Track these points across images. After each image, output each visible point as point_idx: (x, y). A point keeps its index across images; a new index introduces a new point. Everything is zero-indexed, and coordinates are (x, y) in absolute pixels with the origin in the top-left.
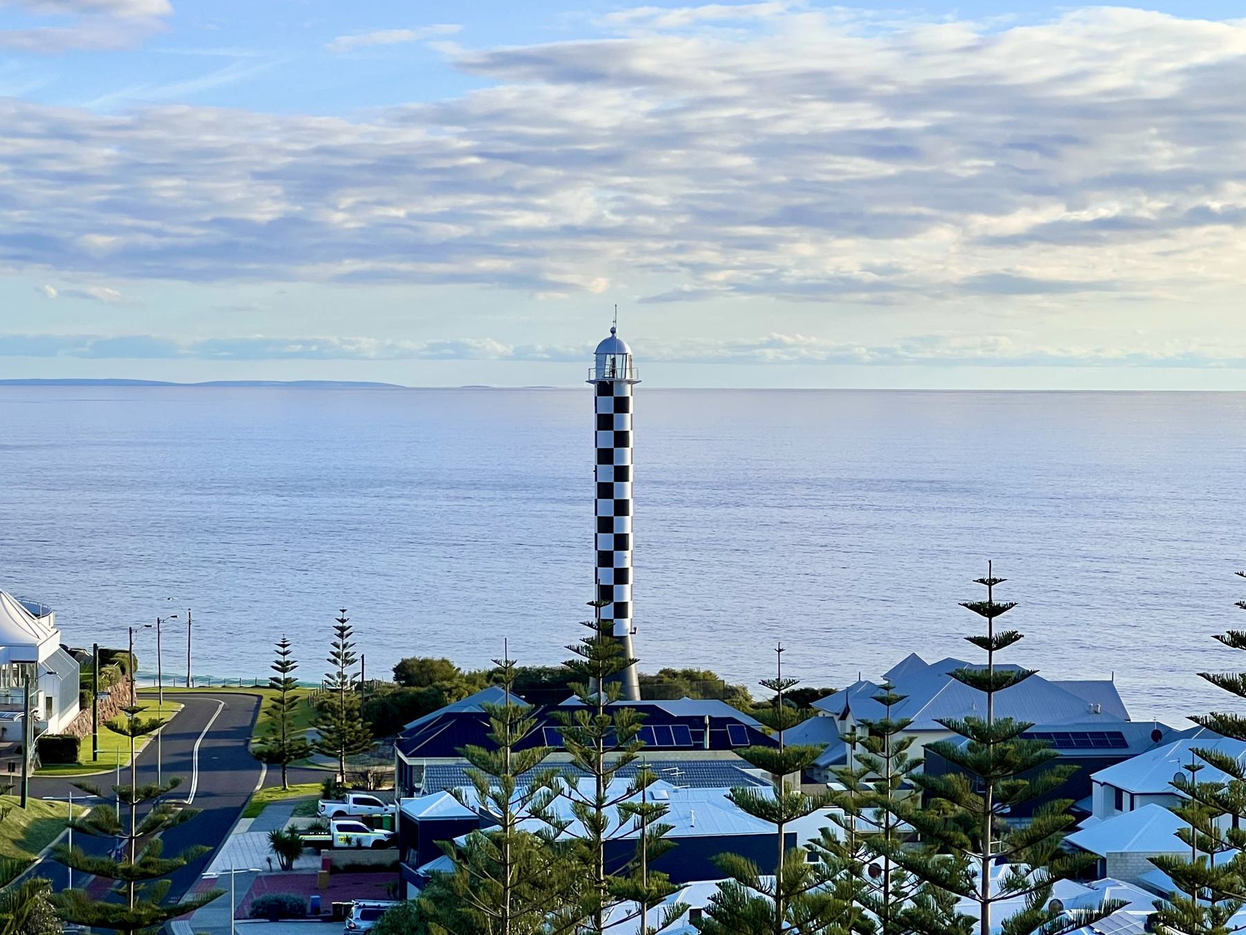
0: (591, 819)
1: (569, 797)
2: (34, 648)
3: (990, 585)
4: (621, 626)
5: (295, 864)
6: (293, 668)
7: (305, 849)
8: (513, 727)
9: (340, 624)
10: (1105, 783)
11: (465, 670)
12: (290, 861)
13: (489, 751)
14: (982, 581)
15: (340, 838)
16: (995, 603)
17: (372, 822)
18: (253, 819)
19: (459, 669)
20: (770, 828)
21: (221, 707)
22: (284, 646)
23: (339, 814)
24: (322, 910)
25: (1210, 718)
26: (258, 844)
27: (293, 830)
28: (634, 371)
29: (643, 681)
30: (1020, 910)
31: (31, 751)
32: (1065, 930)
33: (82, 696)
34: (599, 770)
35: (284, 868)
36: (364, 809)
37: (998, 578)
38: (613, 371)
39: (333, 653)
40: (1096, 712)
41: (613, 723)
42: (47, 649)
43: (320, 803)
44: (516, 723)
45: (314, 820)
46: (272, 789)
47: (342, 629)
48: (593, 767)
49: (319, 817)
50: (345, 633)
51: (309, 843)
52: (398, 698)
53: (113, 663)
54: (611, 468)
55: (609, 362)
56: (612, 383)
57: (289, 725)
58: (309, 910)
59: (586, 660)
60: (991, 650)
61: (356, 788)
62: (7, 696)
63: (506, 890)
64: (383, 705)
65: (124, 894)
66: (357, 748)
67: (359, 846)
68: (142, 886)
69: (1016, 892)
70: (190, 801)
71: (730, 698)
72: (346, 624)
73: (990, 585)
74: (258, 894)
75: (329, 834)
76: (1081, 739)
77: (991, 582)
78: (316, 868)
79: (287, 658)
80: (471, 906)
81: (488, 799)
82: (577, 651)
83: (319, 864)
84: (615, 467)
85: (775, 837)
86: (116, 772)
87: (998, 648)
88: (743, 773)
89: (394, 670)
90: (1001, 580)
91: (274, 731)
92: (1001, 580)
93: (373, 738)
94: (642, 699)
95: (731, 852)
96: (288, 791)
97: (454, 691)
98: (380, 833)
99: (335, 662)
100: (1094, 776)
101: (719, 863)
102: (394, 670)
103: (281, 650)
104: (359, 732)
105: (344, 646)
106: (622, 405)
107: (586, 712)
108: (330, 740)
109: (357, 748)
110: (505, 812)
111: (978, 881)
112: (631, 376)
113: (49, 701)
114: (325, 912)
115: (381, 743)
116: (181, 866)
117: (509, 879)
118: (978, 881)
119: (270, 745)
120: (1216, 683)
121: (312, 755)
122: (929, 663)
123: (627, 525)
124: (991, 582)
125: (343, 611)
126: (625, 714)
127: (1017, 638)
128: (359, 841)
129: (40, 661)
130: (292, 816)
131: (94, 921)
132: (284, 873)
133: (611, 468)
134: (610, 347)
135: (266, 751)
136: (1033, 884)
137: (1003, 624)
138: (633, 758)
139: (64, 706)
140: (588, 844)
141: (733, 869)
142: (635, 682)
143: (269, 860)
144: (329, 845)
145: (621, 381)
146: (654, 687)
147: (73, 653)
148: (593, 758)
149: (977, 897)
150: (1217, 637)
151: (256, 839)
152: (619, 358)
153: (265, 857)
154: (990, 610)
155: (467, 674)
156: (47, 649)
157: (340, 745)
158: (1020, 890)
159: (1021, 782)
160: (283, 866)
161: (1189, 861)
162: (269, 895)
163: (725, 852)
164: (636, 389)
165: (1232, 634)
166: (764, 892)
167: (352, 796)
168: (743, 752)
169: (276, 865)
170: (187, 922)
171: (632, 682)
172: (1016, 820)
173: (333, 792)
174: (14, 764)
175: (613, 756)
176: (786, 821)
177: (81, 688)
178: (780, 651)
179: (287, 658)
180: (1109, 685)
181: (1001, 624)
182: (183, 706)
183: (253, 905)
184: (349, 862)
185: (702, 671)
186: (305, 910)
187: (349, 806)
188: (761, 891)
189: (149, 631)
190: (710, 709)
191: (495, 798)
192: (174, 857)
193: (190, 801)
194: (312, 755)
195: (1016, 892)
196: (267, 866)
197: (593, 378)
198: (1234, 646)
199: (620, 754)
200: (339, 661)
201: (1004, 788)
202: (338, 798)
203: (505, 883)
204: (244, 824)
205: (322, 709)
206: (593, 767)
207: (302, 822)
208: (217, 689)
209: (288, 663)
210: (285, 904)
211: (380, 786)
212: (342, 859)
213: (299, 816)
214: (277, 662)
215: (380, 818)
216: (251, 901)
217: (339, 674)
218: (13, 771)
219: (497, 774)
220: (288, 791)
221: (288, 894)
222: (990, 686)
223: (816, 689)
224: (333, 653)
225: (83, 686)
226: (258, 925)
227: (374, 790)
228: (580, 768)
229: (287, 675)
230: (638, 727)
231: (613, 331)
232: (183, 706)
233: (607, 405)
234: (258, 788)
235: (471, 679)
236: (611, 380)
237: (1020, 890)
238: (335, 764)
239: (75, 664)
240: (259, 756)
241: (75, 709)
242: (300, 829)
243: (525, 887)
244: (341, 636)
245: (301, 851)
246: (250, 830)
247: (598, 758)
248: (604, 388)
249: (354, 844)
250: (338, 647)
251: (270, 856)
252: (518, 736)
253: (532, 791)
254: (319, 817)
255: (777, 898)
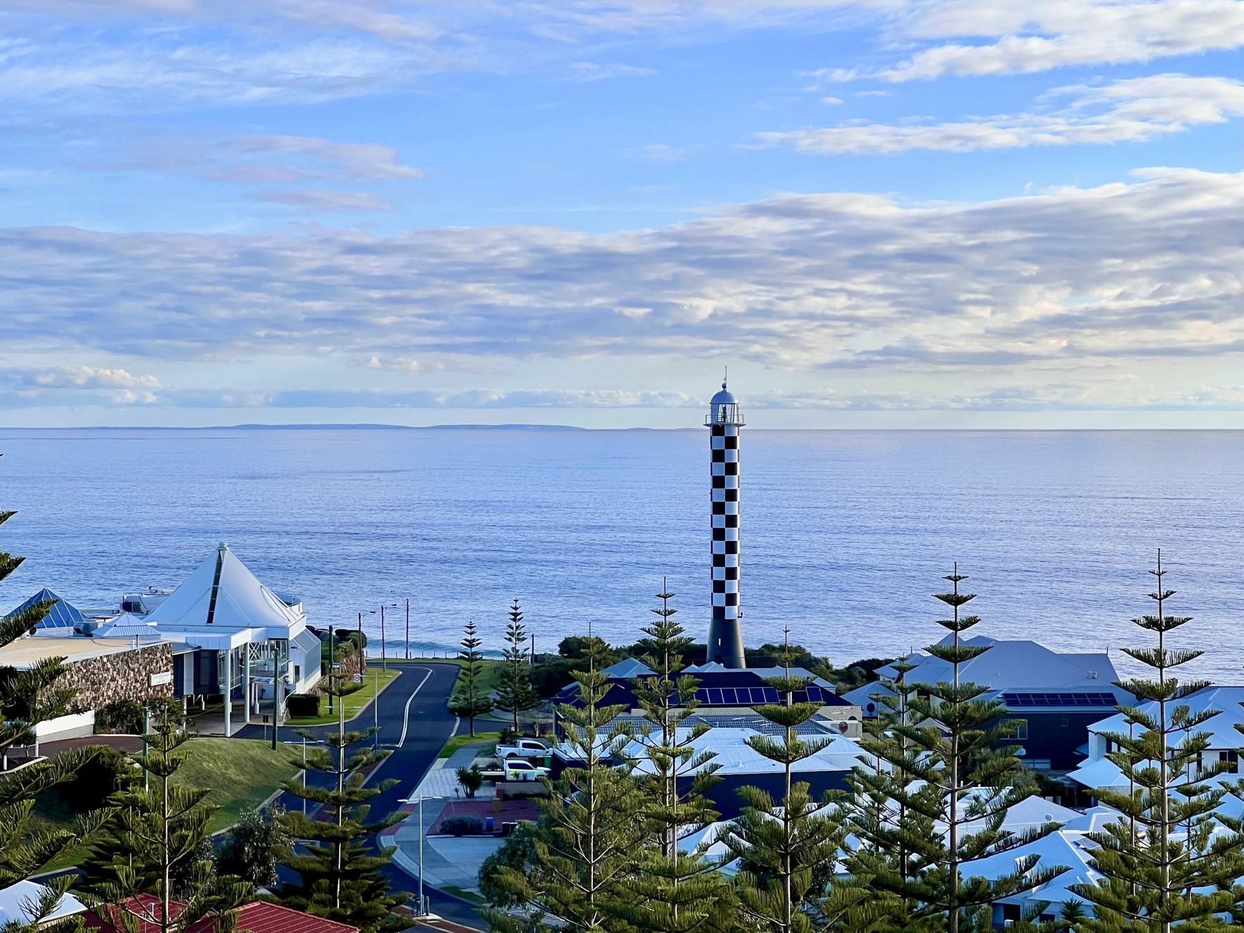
0: (658, 760)
1: (642, 743)
2: (286, 629)
3: (956, 581)
4: (731, 612)
5: (477, 793)
6: (478, 644)
7: (484, 782)
8: (595, 690)
9: (514, 611)
10: (1097, 733)
11: (613, 646)
12: (472, 791)
13: (577, 709)
14: (950, 578)
15: (510, 773)
16: (959, 594)
17: (536, 762)
18: (447, 759)
19: (609, 645)
20: (779, 767)
21: (429, 673)
22: (471, 628)
23: (512, 755)
24: (494, 828)
25: (1130, 683)
26: (449, 778)
27: (475, 768)
28: (740, 417)
29: (748, 653)
30: (981, 830)
31: (282, 707)
32: (1015, 846)
33: (323, 665)
34: (665, 722)
35: (468, 796)
36: (530, 751)
37: (962, 576)
38: (724, 417)
39: (508, 633)
40: (1094, 678)
41: (676, 686)
42: (296, 630)
43: (498, 747)
44: (598, 687)
45: (492, 759)
46: (462, 736)
47: (516, 615)
48: (660, 720)
49: (496, 757)
50: (518, 618)
51: (487, 777)
52: (560, 667)
53: (348, 640)
54: (723, 491)
55: (721, 410)
56: (723, 426)
57: (475, 687)
58: (484, 828)
59: (655, 638)
60: (1161, 631)
61: (526, 736)
62: (265, 665)
63: (590, 814)
64: (549, 673)
65: (335, 815)
66: (527, 705)
67: (525, 780)
68: (350, 810)
69: (976, 817)
70: (400, 745)
71: (814, 666)
72: (518, 611)
73: (956, 581)
74: (447, 816)
75: (503, 770)
76: (1081, 699)
77: (956, 579)
78: (493, 797)
79: (473, 637)
80: (561, 825)
81: (578, 745)
82: (648, 632)
83: (494, 793)
84: (726, 490)
85: (784, 775)
86: (339, 724)
87: (962, 629)
88: (817, 724)
89: (559, 645)
90: (964, 577)
91: (464, 692)
92: (964, 577)
93: (539, 698)
94: (747, 667)
95: (751, 785)
96: (475, 738)
97: (603, 662)
98: (541, 770)
99: (510, 640)
100: (1090, 727)
101: (740, 793)
102: (559, 645)
103: (469, 630)
104: (530, 692)
105: (517, 628)
106: (731, 443)
107: (656, 678)
108: (506, 699)
109: (527, 705)
110: (590, 755)
111: (948, 810)
112: (738, 421)
113: (297, 668)
114: (497, 829)
115: (547, 701)
116: (376, 794)
117: (593, 806)
118: (948, 810)
119: (462, 703)
120: (1134, 656)
121: (492, 710)
122: (965, 640)
123: (734, 534)
124: (956, 579)
125: (516, 601)
126: (685, 680)
127: (976, 622)
128: (525, 776)
129: (290, 639)
130: (476, 756)
131: (311, 836)
132: (468, 800)
133: (723, 491)
134: (722, 398)
135: (458, 707)
136: (989, 811)
137: (964, 610)
138: (691, 713)
139: (309, 673)
140: (657, 779)
141: (751, 799)
142: (742, 655)
143: (457, 790)
144: (502, 779)
145: (730, 425)
146: (762, 657)
147: (317, 633)
148: (660, 713)
149: (947, 820)
150: (1134, 621)
151: (448, 775)
152: (729, 407)
153: (454, 788)
154: (956, 600)
155: (614, 649)
156: (296, 630)
157: (519, 703)
158: (979, 815)
159: (978, 732)
160: (467, 794)
161: (1127, 795)
162: (456, 816)
163: (746, 785)
164: (742, 430)
165: (1147, 618)
166: (774, 816)
167: (521, 742)
168: (760, 708)
169: (462, 794)
170: (392, 836)
171: (739, 655)
172: (1032, 761)
173: (508, 738)
174: (267, 717)
175: (677, 712)
176: (791, 761)
177: (322, 659)
178: (786, 631)
179: (473, 637)
180: (1105, 657)
181: (964, 612)
182: (401, 673)
183: (442, 824)
184: (518, 792)
185: (794, 646)
186: (481, 828)
187: (519, 749)
188: (773, 815)
189: (374, 615)
190: (798, 675)
191: (582, 744)
192: (372, 788)
193: (400, 745)
194: (492, 710)
195: (976, 817)
196: (455, 794)
197: (709, 422)
198: (1148, 628)
199: (681, 710)
200: (513, 639)
201: (965, 736)
202: (511, 743)
203: (589, 809)
204: (440, 762)
205: (505, 674)
206: (660, 720)
207: (482, 762)
208: (429, 659)
209: (474, 640)
210: (466, 823)
211: (544, 733)
212: (511, 790)
213: (482, 756)
214: (466, 640)
215: (543, 759)
216: (442, 821)
217: (513, 649)
218: (267, 721)
219: (583, 725)
220: (475, 738)
221: (469, 816)
222: (956, 658)
223: (881, 659)
224: (508, 633)
225: (323, 657)
226: (444, 840)
227: (539, 737)
228: (651, 721)
229: (474, 649)
230: (694, 690)
231: (724, 387)
232: (401, 673)
233: (720, 443)
234: (452, 735)
235: (618, 652)
236: (723, 423)
237: (979, 815)
238: (510, 717)
239: (317, 641)
240: (452, 711)
241: (317, 676)
242: (480, 766)
243: (608, 812)
244: (514, 620)
245: (481, 784)
246: (444, 767)
247: (664, 712)
248: (718, 430)
249: (521, 778)
250: (512, 628)
251: (458, 787)
252: (599, 697)
253: (611, 738)
254: (496, 757)
255: (786, 820)
